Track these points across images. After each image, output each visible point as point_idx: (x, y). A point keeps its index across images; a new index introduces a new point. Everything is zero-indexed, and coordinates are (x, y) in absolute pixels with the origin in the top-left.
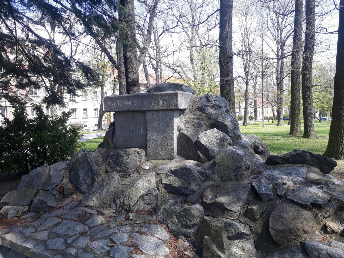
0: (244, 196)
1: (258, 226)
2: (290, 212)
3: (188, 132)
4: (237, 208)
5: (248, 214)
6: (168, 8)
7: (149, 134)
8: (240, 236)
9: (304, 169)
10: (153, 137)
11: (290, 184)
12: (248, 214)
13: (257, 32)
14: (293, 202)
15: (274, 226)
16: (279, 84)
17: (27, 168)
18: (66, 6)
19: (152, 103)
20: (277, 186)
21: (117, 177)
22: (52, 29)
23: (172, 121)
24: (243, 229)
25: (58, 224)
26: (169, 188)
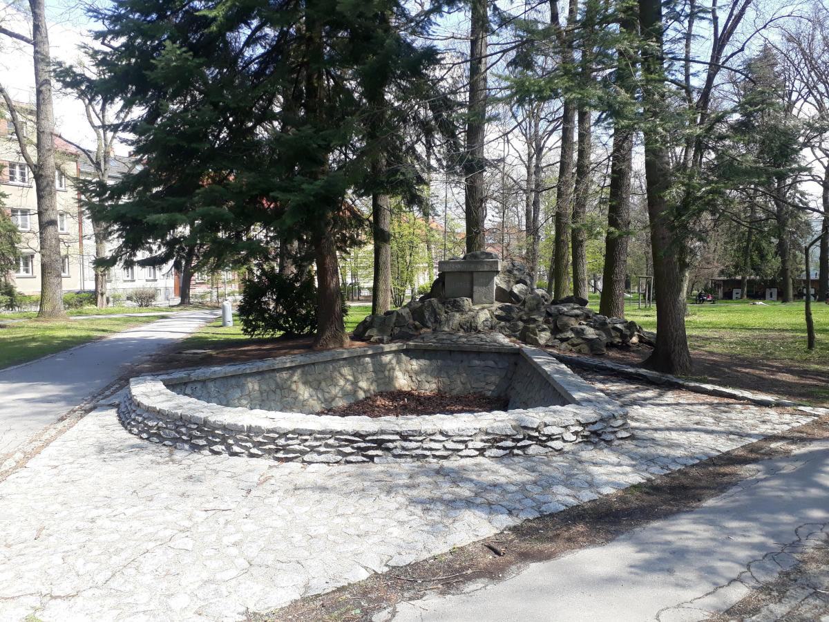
0: (544, 315)
1: (552, 326)
2: (565, 319)
3: (504, 286)
4: (541, 319)
5: (546, 322)
6: (684, 42)
7: (475, 288)
8: (544, 330)
9: (572, 304)
10: (477, 290)
11: (565, 309)
12: (546, 322)
13: (605, 190)
14: (567, 315)
15: (559, 324)
16: (532, 229)
17: (218, 227)
18: (318, 355)
19: (479, 266)
20: (559, 311)
21: (457, 315)
22: (701, 568)
23: (493, 278)
24: (545, 326)
25: (451, 352)
26: (498, 317)
